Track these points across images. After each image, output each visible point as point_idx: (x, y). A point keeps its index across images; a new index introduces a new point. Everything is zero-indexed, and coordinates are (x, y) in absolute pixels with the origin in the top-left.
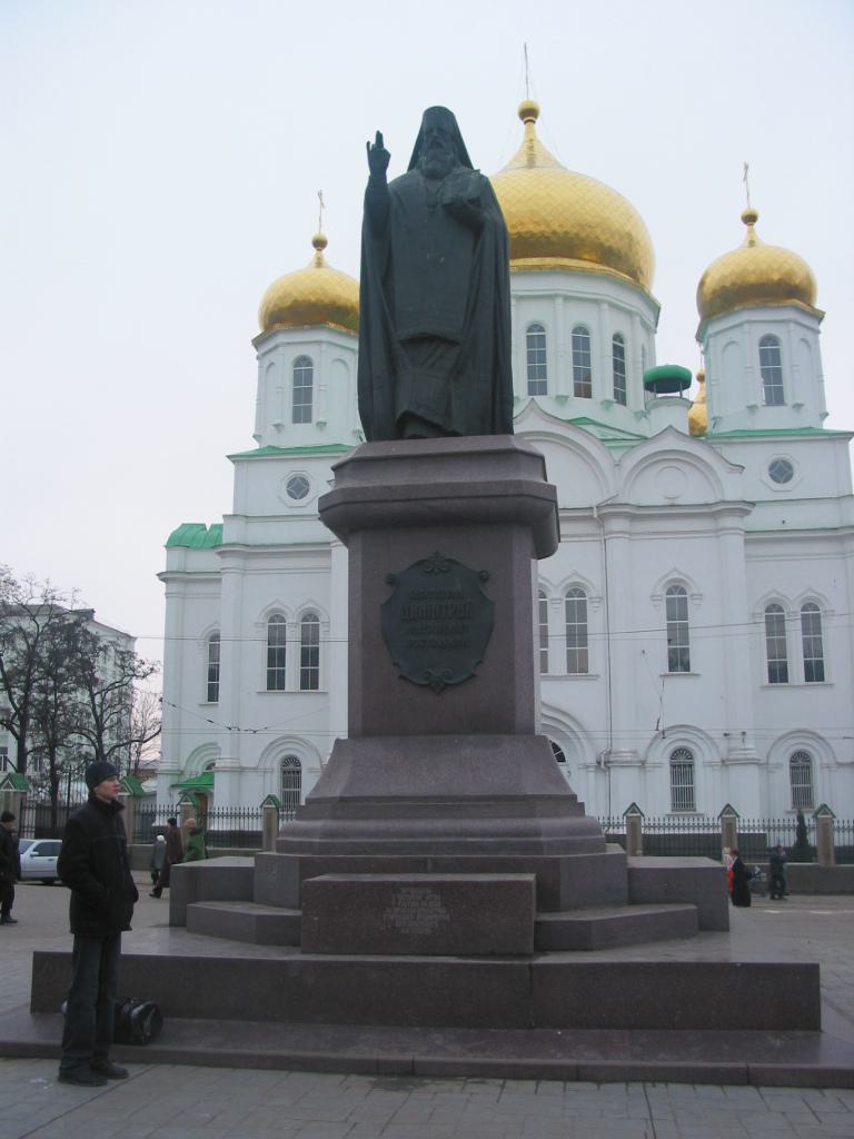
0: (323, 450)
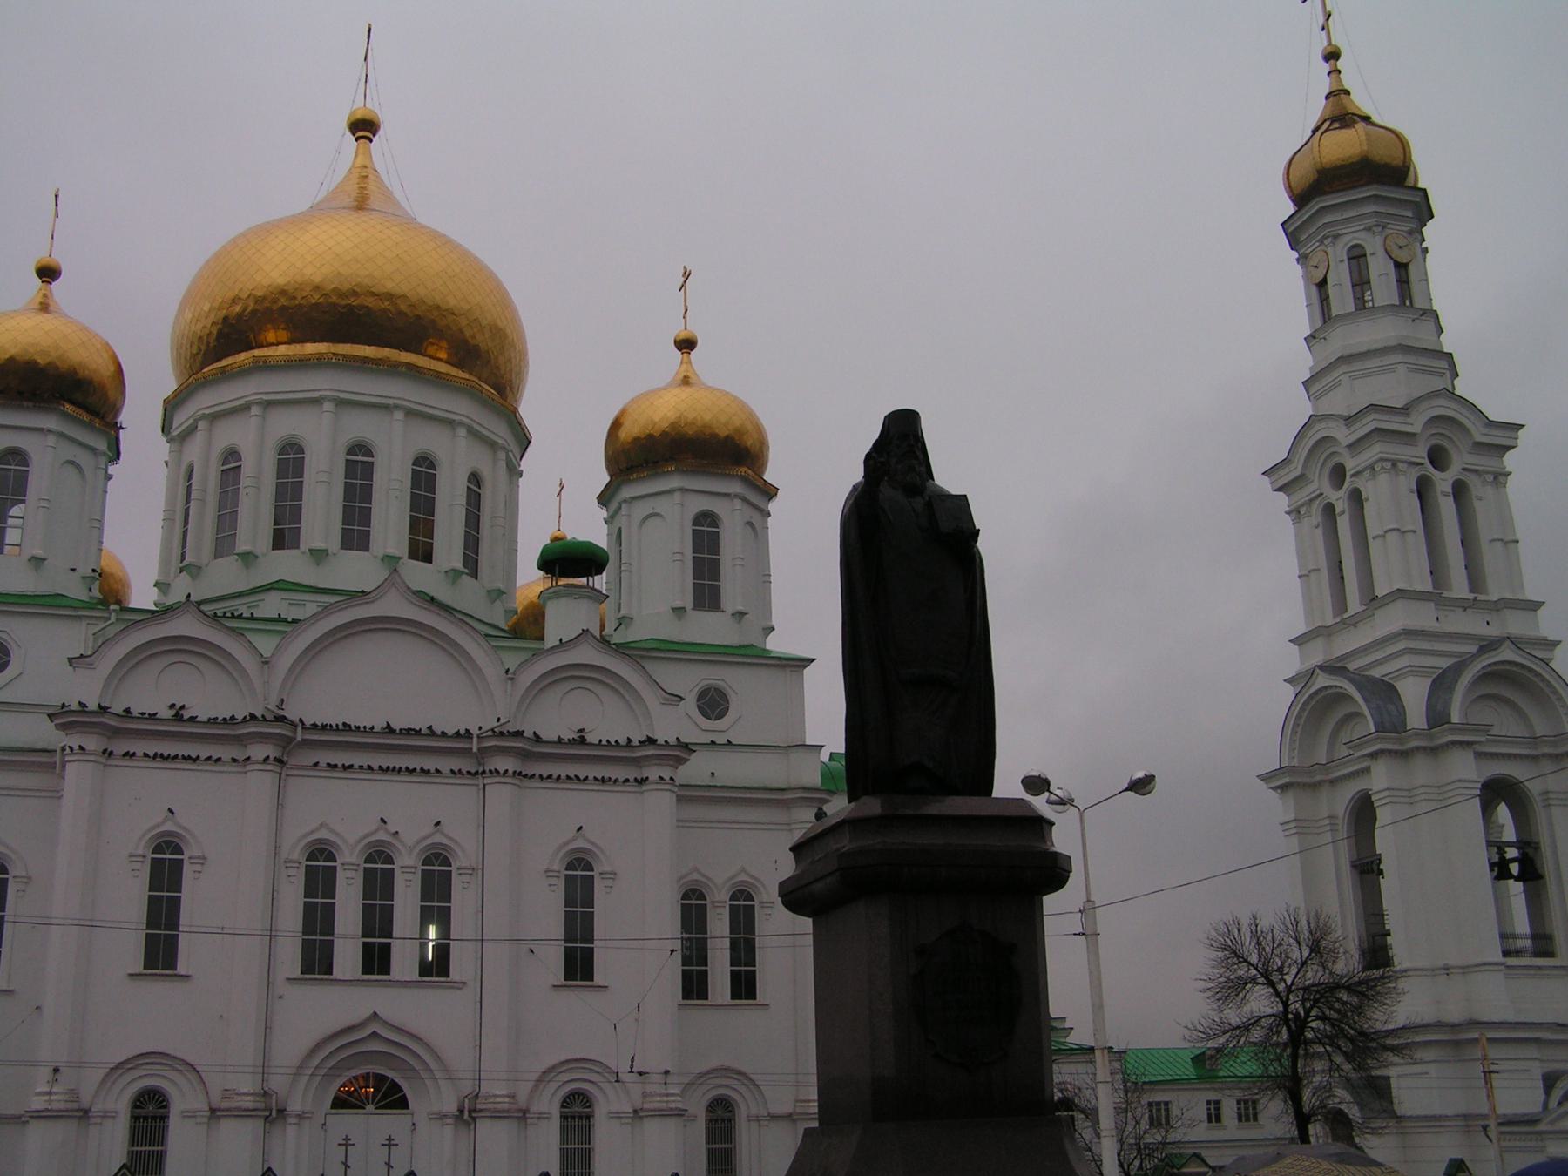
0: (58, 601)
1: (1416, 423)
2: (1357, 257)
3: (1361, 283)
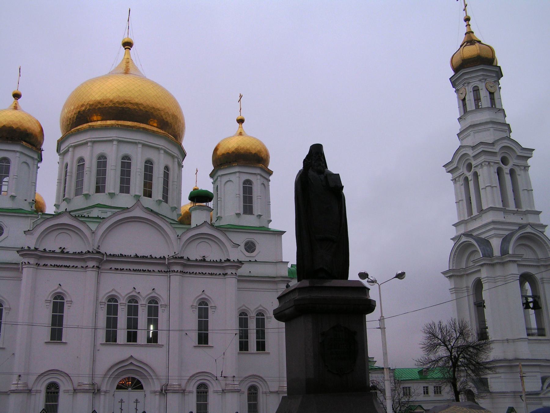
1: (497, 149)
2: (476, 90)
3: (477, 99)
